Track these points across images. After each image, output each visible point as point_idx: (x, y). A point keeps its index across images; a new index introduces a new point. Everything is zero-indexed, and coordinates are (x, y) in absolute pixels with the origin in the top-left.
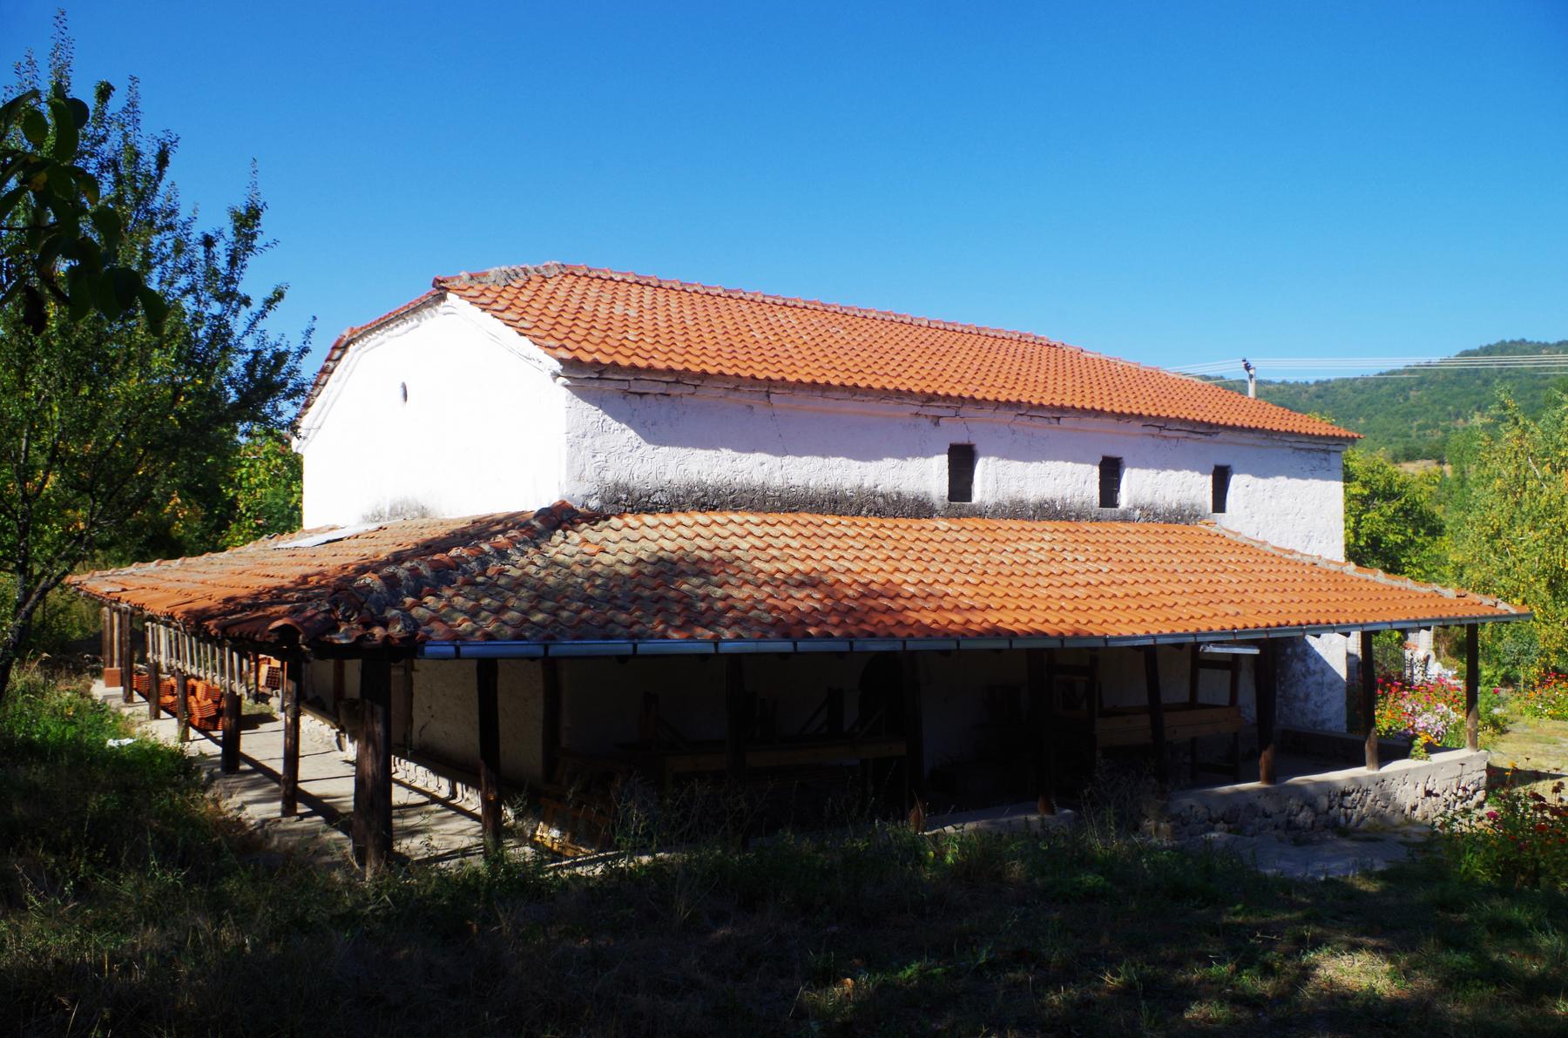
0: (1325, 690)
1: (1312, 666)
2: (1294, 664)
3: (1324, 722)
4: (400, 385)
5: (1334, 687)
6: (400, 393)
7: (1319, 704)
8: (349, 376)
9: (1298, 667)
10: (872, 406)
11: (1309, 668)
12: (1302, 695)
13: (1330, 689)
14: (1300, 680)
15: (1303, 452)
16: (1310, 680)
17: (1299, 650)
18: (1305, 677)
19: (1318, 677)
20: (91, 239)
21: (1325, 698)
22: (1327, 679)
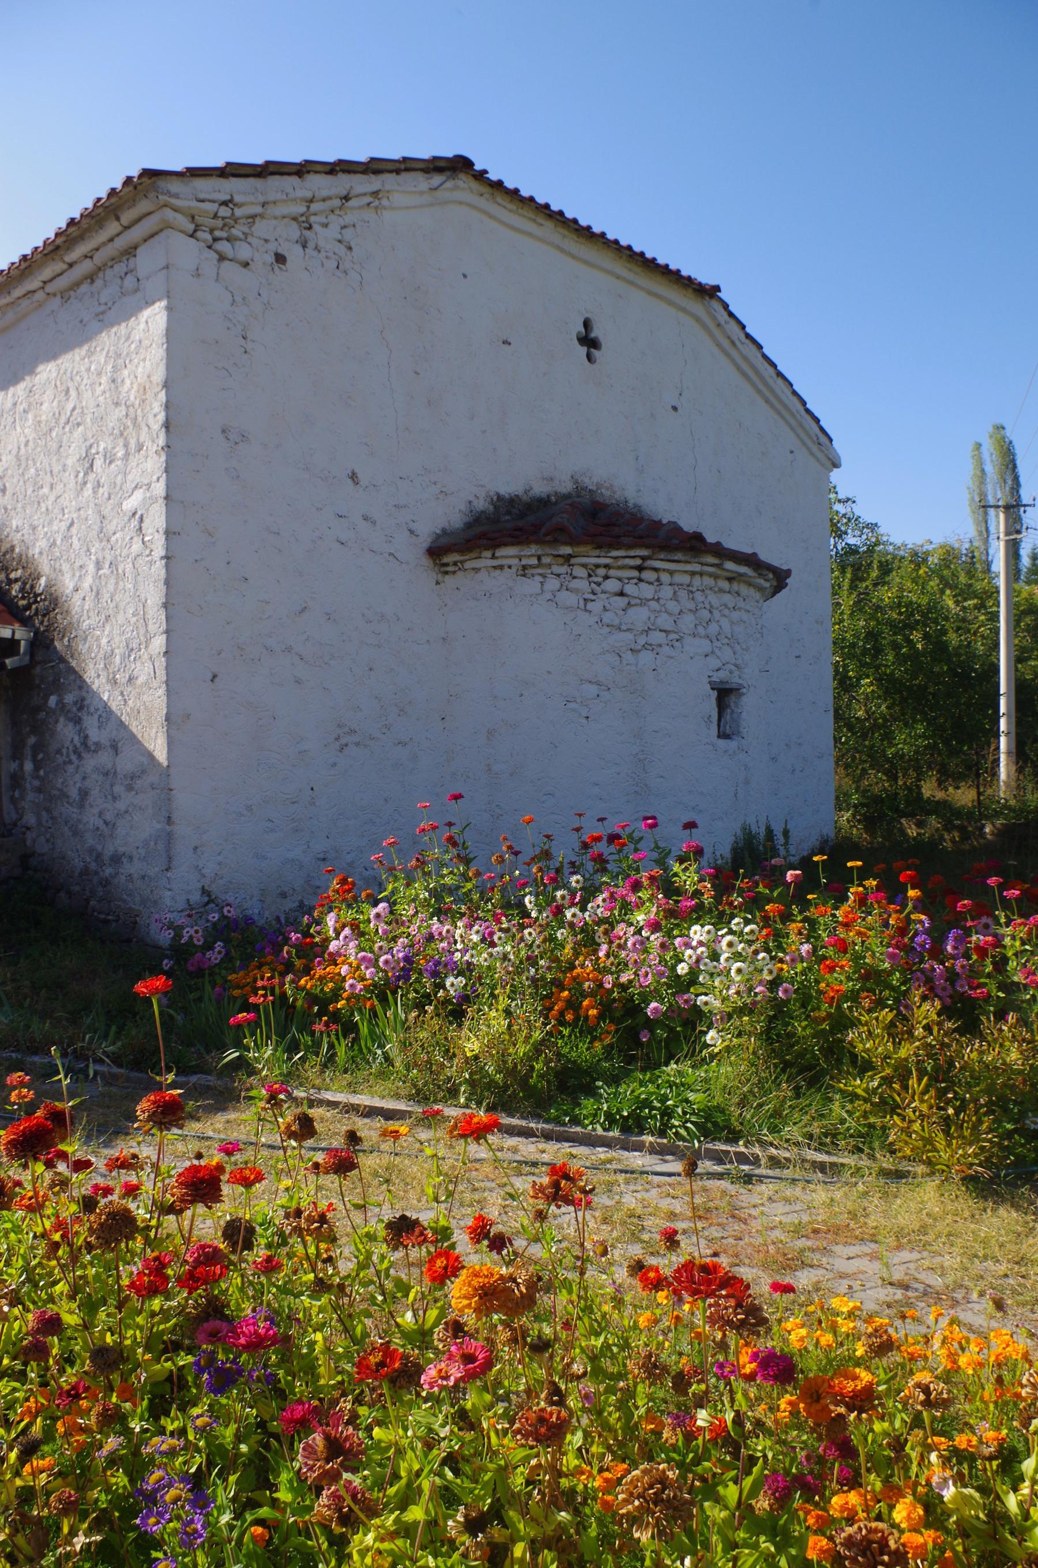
0: (118, 789)
1: (94, 734)
2: (60, 726)
3: (116, 859)
4: (971, 447)
5: (139, 784)
6: (216, 680)
7: (108, 817)
8: (469, 205)
9: (65, 731)
10: (645, 280)
11: (86, 737)
12: (74, 793)
13: (130, 788)
14: (70, 762)
15: (84, 288)
16: (90, 763)
17: (69, 698)
18: (80, 757)
19: (104, 758)
20: (237, 1483)
21: (121, 806)
22: (125, 763)
